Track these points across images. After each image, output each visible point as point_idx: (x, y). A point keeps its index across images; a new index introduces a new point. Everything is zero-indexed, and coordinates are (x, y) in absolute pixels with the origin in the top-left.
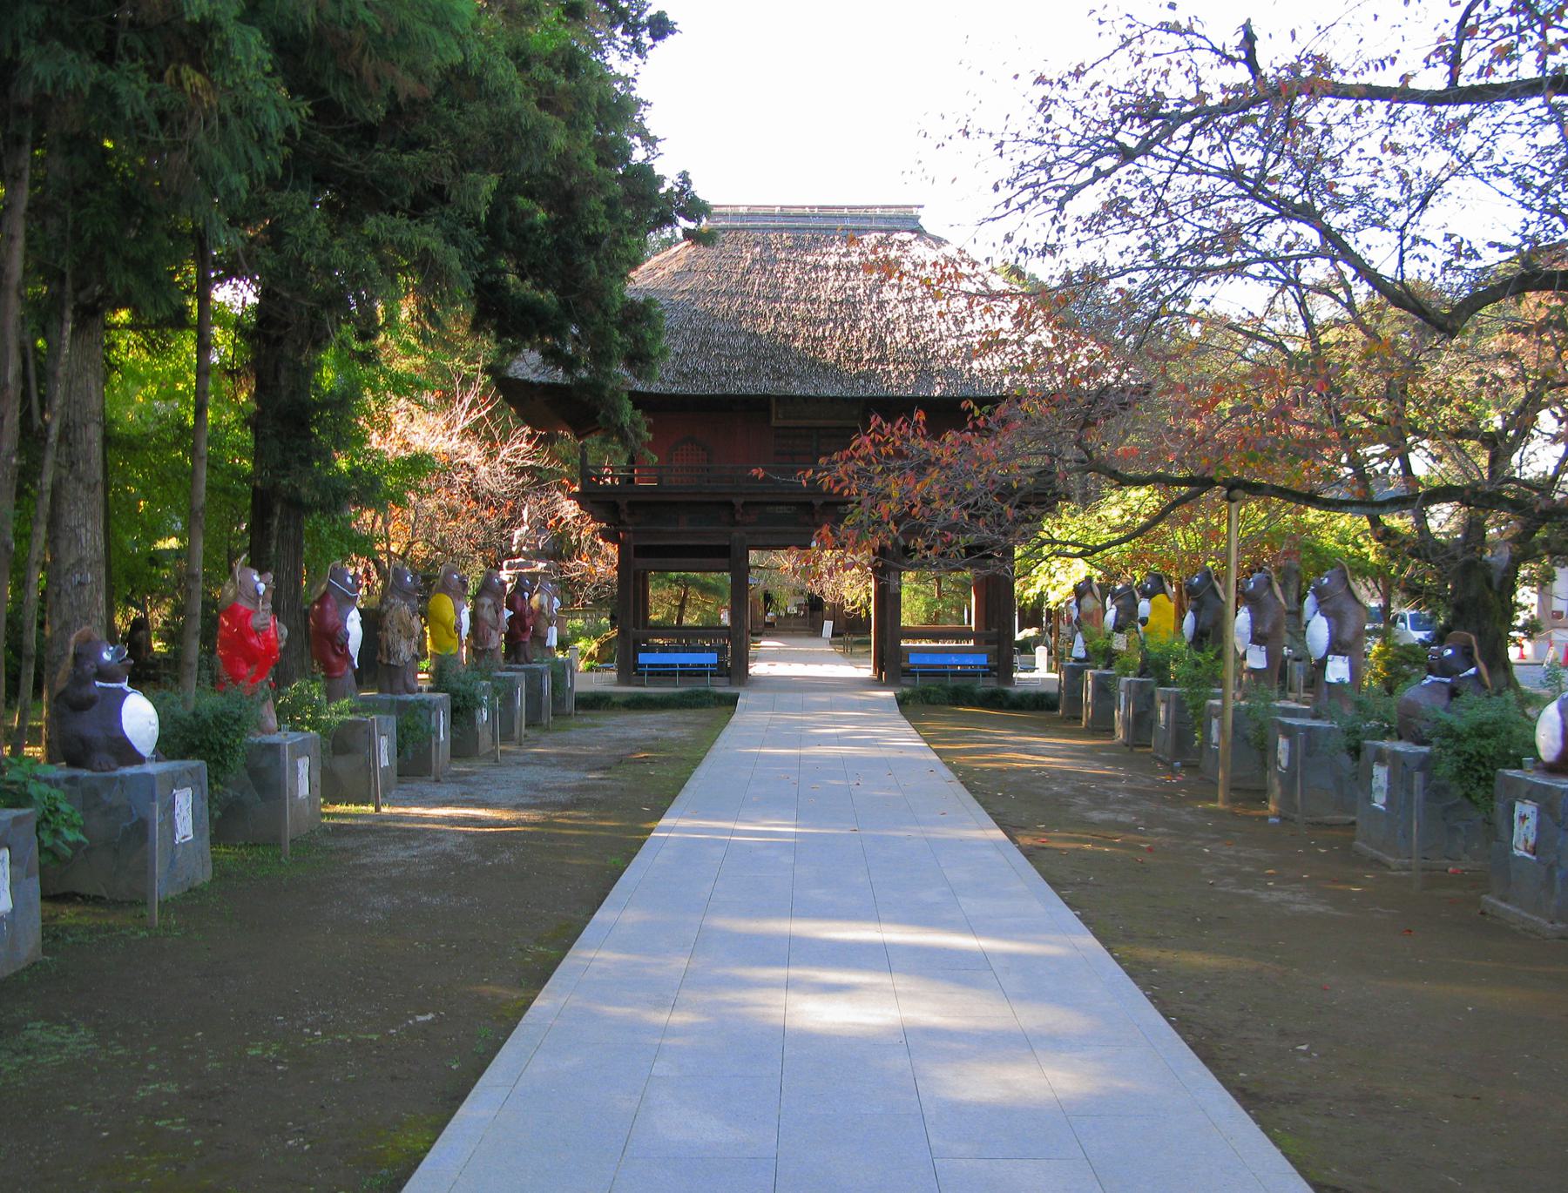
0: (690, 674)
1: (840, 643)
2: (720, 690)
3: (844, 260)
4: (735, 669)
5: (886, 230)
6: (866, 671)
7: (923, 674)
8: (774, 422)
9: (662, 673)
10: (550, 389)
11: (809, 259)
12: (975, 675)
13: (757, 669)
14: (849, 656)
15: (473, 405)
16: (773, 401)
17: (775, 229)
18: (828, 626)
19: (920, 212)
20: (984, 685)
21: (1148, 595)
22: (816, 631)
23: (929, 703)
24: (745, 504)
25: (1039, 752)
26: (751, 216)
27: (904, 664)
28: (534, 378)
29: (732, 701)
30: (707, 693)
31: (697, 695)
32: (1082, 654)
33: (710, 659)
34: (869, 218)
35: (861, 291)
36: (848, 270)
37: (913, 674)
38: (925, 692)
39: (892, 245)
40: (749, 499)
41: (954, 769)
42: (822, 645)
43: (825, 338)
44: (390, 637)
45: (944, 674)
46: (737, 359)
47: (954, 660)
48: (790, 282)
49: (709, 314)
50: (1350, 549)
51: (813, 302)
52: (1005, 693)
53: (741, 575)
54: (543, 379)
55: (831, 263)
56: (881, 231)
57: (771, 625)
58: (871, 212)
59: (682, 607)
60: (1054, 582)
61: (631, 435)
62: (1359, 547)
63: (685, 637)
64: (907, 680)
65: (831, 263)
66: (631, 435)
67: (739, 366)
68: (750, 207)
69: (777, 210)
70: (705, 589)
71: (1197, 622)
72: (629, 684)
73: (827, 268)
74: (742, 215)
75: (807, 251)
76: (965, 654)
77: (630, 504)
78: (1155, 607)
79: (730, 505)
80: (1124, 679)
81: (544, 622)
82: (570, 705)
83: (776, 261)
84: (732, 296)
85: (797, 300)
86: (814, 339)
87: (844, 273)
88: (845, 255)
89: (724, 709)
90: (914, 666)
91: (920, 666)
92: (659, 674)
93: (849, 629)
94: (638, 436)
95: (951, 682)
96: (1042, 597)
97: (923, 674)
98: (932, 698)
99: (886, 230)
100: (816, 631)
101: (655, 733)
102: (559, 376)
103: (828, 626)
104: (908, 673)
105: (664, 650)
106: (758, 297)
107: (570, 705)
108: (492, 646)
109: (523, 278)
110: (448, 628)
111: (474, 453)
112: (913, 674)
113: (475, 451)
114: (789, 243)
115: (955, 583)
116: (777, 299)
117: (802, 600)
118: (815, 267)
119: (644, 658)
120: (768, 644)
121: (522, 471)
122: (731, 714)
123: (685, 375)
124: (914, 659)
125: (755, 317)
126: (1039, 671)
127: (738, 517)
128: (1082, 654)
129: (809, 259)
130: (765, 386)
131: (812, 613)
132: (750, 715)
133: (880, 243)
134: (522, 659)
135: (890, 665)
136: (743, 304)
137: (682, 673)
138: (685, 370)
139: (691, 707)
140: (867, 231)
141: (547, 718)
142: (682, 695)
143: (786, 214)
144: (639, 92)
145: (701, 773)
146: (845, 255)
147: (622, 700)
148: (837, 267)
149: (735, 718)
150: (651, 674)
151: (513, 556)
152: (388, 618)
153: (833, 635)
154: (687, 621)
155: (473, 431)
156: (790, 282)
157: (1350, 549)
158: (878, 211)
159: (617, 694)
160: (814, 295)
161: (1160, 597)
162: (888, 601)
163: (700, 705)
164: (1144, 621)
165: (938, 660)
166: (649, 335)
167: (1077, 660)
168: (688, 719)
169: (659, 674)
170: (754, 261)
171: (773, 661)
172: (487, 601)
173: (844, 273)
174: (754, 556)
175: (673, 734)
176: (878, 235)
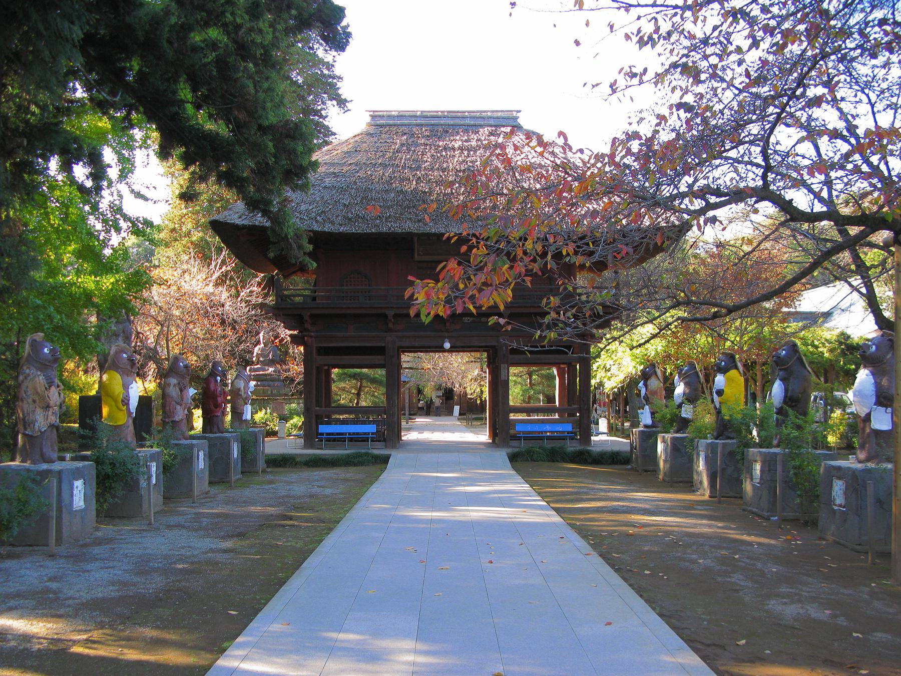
0: (357, 440)
1: (464, 419)
2: (376, 452)
3: (466, 144)
4: (390, 435)
5: (495, 126)
6: (484, 437)
7: (526, 438)
8: (416, 258)
9: (335, 440)
10: (253, 231)
11: (441, 143)
12: (564, 439)
13: (409, 436)
14: (470, 427)
15: (224, 263)
16: (416, 239)
17: (417, 125)
18: (457, 409)
19: (518, 114)
20: (572, 447)
21: (724, 371)
22: (450, 413)
23: (533, 460)
24: (396, 316)
25: (648, 510)
26: (401, 116)
27: (512, 432)
28: (239, 222)
29: (385, 460)
30: (367, 454)
31: (359, 455)
32: (649, 421)
33: (371, 428)
34: (483, 118)
35: (478, 163)
36: (469, 150)
37: (519, 439)
38: (530, 454)
39: (499, 135)
40: (398, 312)
41: (583, 532)
42: (452, 421)
43: (452, 193)
44: (25, 406)
45: (541, 438)
46: (389, 208)
47: (548, 428)
48: (427, 157)
49: (368, 179)
50: (811, 349)
51: (444, 170)
52: (589, 452)
53: (394, 372)
54: (246, 222)
55: (456, 146)
56: (491, 126)
57: (422, 408)
58: (484, 114)
59: (358, 394)
60: (609, 374)
61: (294, 246)
62: (816, 347)
63: (359, 414)
64: (514, 443)
65: (456, 146)
66: (294, 246)
67: (391, 212)
68: (399, 112)
69: (418, 113)
70: (373, 381)
71: (786, 390)
72: (312, 447)
73: (454, 149)
74: (394, 117)
75: (439, 138)
76: (553, 424)
77: (311, 316)
78: (729, 381)
79: (385, 316)
80: (703, 442)
81: (241, 402)
82: (261, 464)
83: (417, 145)
84: (385, 166)
85: (432, 169)
86: (445, 195)
87: (466, 153)
88: (466, 141)
89: (378, 466)
90: (519, 432)
91: (524, 432)
92: (334, 440)
93: (472, 411)
94: (300, 247)
95: (548, 445)
96: (601, 384)
97: (526, 438)
98: (535, 456)
99: (495, 126)
100: (450, 413)
101: (315, 490)
102: (259, 219)
103: (457, 409)
104: (515, 438)
105: (344, 422)
106: (404, 167)
107: (261, 464)
108: (177, 418)
109: (198, 107)
110: (116, 401)
111: (224, 294)
112: (519, 439)
113: (225, 295)
114: (427, 133)
115: (542, 376)
116: (418, 168)
117: (440, 393)
118: (445, 148)
119: (323, 429)
120: (420, 420)
121: (255, 307)
122: (383, 471)
123: (350, 219)
124: (519, 428)
125: (402, 180)
126: (602, 435)
127: (390, 325)
128: (649, 421)
129: (441, 143)
130: (409, 226)
131: (448, 402)
132: (397, 473)
133: (491, 134)
134: (216, 430)
135: (501, 432)
136: (394, 172)
137: (351, 440)
138: (350, 215)
139: (355, 465)
140: (482, 126)
141: (235, 476)
142: (348, 456)
143: (424, 116)
144: (337, 71)
145: (331, 541)
146: (466, 141)
147: (303, 460)
148: (461, 149)
149: (385, 475)
150: (328, 440)
151: (253, 363)
152: (23, 387)
153: (460, 414)
154: (364, 404)
155: (220, 282)
156: (427, 157)
157: (811, 349)
158: (489, 114)
159: (301, 455)
160: (445, 165)
161: (733, 373)
162: (499, 387)
163: (361, 464)
164: (720, 393)
165: (537, 428)
166: (300, 149)
167: (646, 426)
168: (349, 475)
169: (334, 440)
170: (402, 145)
171: (420, 432)
172: (173, 381)
173: (466, 153)
174: (406, 359)
175: (328, 491)
176: (490, 129)
